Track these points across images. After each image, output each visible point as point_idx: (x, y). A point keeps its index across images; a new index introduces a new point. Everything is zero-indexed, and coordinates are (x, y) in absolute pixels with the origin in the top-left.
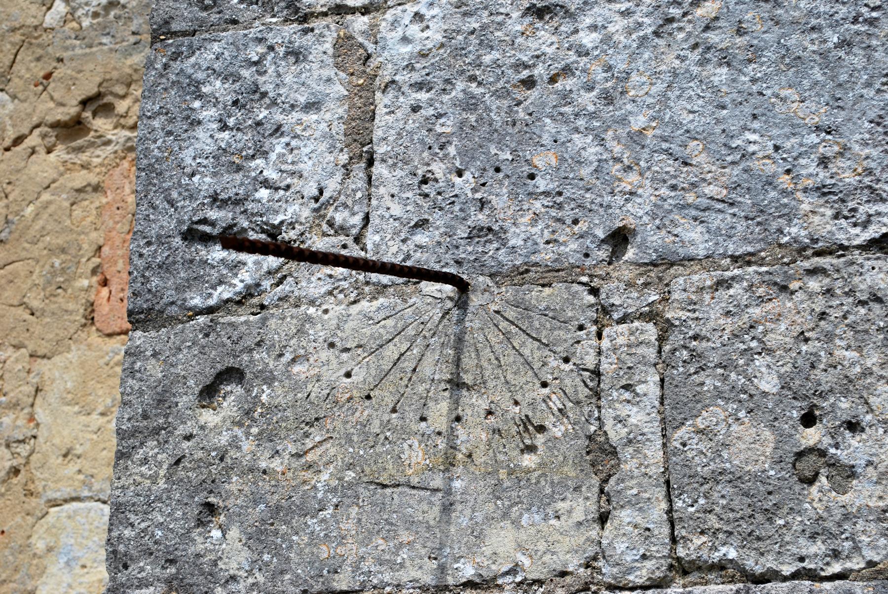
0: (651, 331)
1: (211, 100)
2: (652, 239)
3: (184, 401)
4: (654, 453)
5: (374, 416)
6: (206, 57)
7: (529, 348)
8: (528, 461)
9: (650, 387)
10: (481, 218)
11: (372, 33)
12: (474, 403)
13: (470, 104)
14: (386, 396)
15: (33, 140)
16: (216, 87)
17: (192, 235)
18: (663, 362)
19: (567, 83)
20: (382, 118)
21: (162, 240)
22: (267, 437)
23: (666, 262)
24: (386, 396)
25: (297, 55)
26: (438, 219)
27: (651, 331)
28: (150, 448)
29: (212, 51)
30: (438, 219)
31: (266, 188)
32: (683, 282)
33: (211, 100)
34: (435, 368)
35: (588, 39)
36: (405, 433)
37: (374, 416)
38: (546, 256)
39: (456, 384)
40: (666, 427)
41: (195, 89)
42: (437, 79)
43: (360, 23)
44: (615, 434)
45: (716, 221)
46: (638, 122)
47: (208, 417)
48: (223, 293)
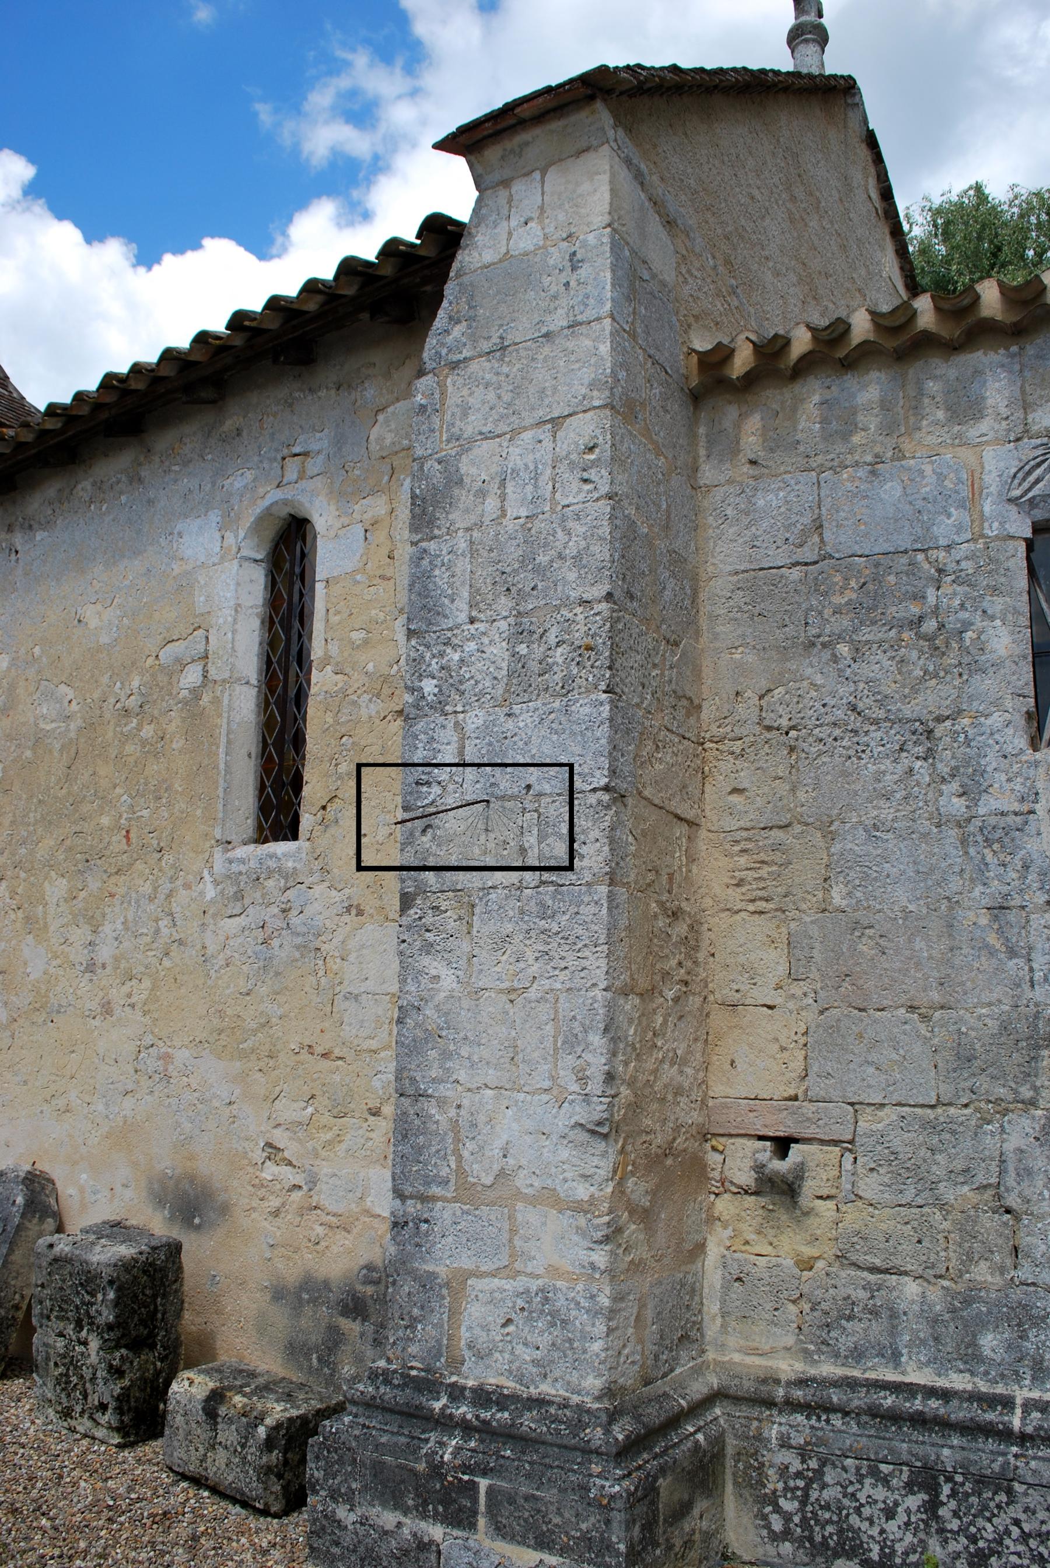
0: (536, 815)
1: (421, 741)
2: (536, 788)
3: (417, 834)
4: (536, 850)
5: (466, 839)
6: (419, 727)
7: (505, 820)
8: (505, 852)
9: (535, 832)
10: (493, 780)
11: (464, 720)
12: (492, 836)
13: (490, 744)
14: (469, 833)
15: (389, 717)
16: (422, 737)
17: (417, 783)
18: (539, 824)
19: (515, 739)
20: (467, 748)
21: (410, 785)
22: (439, 845)
23: (540, 795)
24: (469, 833)
25: (444, 727)
26: (482, 780)
27: (536, 815)
28: (409, 848)
29: (421, 725)
30: (482, 780)
31: (696, 470)
32: (544, 801)
33: (421, 741)
34: (481, 826)
35: (521, 724)
36: (474, 844)
37: (466, 839)
38: (509, 793)
39: (487, 830)
40: (540, 843)
41: (416, 737)
42: (481, 736)
43: (461, 716)
44: (527, 845)
45: (553, 782)
46: (534, 752)
47: (424, 839)
48: (426, 802)
